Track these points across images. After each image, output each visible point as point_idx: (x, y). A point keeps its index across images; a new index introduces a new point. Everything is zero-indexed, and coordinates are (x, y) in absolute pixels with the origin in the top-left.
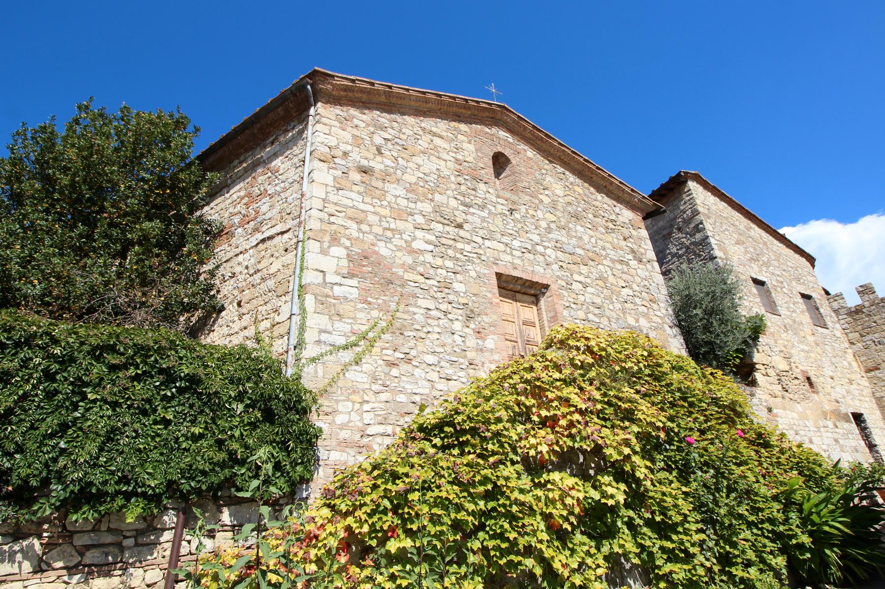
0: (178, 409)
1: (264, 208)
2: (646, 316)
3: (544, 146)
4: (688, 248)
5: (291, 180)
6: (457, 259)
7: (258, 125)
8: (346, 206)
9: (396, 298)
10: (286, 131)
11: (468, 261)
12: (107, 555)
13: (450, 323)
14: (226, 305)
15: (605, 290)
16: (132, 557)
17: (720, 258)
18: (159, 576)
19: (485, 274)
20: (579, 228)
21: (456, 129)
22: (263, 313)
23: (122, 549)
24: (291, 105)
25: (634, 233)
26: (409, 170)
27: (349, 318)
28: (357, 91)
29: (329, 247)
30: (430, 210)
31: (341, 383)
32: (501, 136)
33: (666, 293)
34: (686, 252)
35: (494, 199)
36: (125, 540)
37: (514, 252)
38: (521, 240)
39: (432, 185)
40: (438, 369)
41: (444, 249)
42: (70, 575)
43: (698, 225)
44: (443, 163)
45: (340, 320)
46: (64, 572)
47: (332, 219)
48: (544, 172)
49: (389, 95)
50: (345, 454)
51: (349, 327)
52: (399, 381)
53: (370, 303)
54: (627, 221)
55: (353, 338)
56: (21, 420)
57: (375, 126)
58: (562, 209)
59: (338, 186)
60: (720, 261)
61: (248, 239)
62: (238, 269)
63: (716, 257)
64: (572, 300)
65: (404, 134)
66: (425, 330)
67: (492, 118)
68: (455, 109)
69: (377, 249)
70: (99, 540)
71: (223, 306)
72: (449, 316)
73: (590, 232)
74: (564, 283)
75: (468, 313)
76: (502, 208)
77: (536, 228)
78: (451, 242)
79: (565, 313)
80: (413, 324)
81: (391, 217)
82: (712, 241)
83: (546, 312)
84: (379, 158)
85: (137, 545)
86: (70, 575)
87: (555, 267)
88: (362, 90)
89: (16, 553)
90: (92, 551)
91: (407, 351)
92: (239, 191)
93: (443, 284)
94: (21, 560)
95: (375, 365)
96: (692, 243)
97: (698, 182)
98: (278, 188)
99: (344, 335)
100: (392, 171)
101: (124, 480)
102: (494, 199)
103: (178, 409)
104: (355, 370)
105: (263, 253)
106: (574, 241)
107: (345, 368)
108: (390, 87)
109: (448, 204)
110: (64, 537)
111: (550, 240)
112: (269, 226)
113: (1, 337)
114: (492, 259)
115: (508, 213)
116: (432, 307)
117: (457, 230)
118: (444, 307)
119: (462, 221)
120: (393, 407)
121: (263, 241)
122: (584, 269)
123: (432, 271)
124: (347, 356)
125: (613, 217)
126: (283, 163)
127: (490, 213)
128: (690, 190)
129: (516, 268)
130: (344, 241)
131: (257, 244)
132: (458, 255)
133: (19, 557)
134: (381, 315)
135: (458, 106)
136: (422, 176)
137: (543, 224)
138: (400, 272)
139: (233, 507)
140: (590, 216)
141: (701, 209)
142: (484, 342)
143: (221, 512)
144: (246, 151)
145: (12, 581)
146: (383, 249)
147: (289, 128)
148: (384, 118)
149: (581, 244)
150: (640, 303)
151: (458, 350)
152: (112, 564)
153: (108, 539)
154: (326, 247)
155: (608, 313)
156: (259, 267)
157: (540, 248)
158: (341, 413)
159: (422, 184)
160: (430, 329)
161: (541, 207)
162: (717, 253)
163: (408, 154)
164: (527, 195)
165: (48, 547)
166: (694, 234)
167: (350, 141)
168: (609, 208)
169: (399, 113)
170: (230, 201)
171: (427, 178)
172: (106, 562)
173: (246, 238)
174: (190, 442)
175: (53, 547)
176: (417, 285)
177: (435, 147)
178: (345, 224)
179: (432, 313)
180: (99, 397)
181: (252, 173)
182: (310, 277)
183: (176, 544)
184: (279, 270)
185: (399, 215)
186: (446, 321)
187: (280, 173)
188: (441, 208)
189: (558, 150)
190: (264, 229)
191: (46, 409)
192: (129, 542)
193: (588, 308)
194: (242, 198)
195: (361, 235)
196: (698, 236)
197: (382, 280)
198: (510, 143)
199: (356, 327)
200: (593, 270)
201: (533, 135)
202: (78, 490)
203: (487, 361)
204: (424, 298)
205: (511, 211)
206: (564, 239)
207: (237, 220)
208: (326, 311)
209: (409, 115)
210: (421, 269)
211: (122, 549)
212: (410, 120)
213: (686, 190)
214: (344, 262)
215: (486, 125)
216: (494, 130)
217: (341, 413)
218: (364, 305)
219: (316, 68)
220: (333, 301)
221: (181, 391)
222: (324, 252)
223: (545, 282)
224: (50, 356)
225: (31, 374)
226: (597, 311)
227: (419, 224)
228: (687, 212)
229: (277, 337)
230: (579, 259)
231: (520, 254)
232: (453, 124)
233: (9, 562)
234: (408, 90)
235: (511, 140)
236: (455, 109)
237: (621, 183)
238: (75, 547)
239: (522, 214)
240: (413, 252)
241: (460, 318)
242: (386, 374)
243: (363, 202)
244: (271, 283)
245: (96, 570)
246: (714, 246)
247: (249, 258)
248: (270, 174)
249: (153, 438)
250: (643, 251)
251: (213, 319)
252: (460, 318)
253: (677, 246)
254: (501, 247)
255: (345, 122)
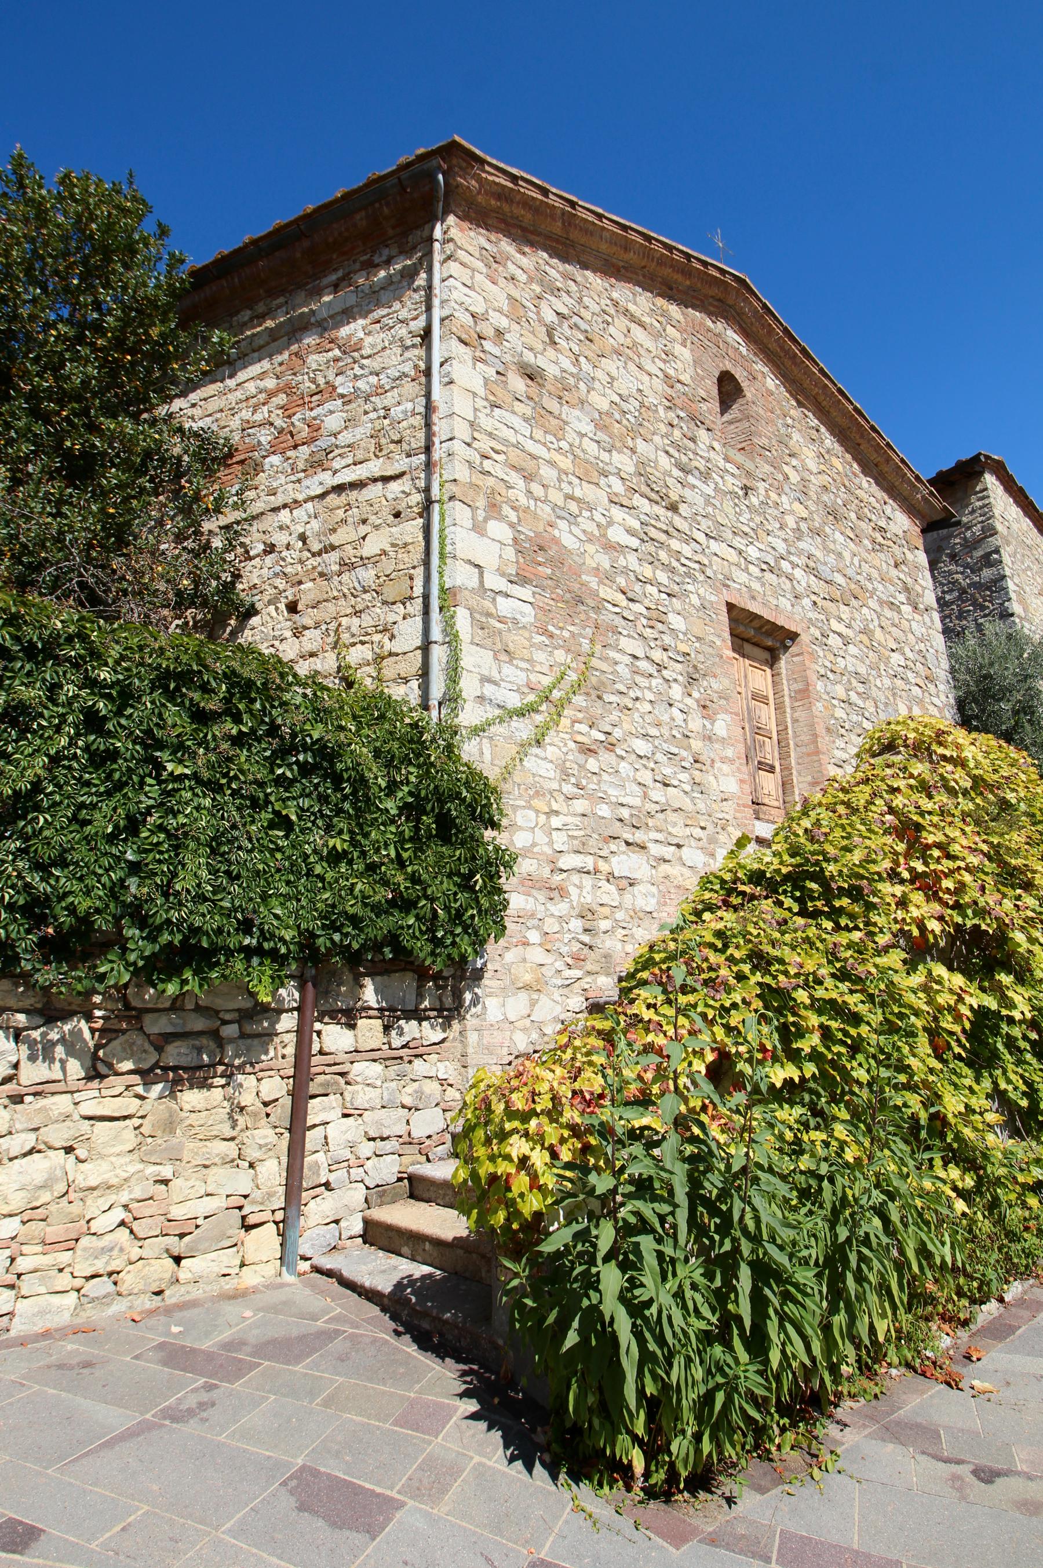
0: (306, 803)
1: (333, 423)
2: (920, 702)
3: (796, 370)
4: (963, 591)
5: (394, 373)
6: (673, 571)
7: (306, 243)
8: (505, 442)
9: (589, 631)
10: (371, 266)
11: (688, 575)
12: (199, 1050)
13: (666, 686)
14: (259, 606)
15: (871, 654)
16: (238, 1056)
17: (1019, 617)
18: (280, 1090)
19: (711, 603)
20: (837, 535)
21: (664, 314)
22: (354, 630)
23: (221, 1043)
24: (386, 211)
25: (909, 556)
26: (597, 385)
27: (522, 659)
28: (518, 203)
29: (486, 520)
30: (632, 469)
31: (517, 777)
32: (729, 340)
33: (947, 667)
34: (959, 598)
35: (721, 463)
36: (224, 1027)
37: (751, 567)
38: (762, 547)
39: (632, 420)
40: (652, 765)
41: (653, 549)
42: (147, 1084)
43: (990, 553)
44: (646, 378)
45: (510, 662)
46: (136, 1079)
47: (487, 465)
48: (790, 421)
49: (570, 220)
50: (531, 900)
51: (523, 675)
52: (599, 782)
53: (551, 636)
54: (901, 534)
55: (531, 698)
56: (55, 804)
57: (541, 283)
58: (815, 498)
59: (492, 398)
60: (1017, 620)
61: (299, 481)
62: (280, 539)
63: (1012, 615)
64: (829, 665)
65: (586, 307)
66: (632, 694)
67: (720, 300)
68: (667, 271)
69: (556, 533)
70: (184, 1024)
71: (253, 605)
72: (665, 672)
73: (851, 545)
74: (818, 634)
75: (691, 670)
76: (732, 483)
77: (781, 528)
78: (663, 537)
79: (820, 686)
80: (614, 682)
81: (574, 474)
82: (1011, 585)
83: (788, 680)
84: (551, 352)
85: (243, 1035)
86: (147, 1084)
87: (806, 602)
88: (527, 203)
89: (54, 1044)
90: (176, 1044)
91: (608, 729)
92: (262, 376)
93: (654, 614)
94: (64, 1056)
95: (564, 750)
96: (973, 585)
97: (998, 478)
98: (361, 384)
99: (517, 691)
100: (572, 381)
101: (246, 926)
102: (721, 463)
103: (306, 803)
104: (536, 756)
105: (340, 513)
106: (831, 559)
107: (524, 747)
108: (573, 204)
109: (656, 462)
110: (128, 1019)
111: (800, 553)
112: (350, 461)
113: (3, 637)
114: (721, 577)
115: (741, 493)
116: (640, 654)
117: (669, 514)
118: (658, 655)
119: (677, 498)
120: (593, 824)
121: (339, 489)
122: (845, 612)
123: (637, 587)
124: (523, 729)
125: (882, 523)
126: (369, 334)
127: (716, 489)
128: (986, 489)
129: (753, 598)
130: (506, 510)
131: (322, 496)
132: (675, 564)
133: (60, 1051)
134: (569, 660)
135: (673, 265)
136: (617, 399)
137: (790, 521)
138: (593, 583)
139: (378, 978)
140: (853, 516)
141: (999, 527)
142: (712, 724)
143: (362, 986)
144: (272, 294)
145: (53, 1094)
146: (567, 536)
147: (377, 260)
148: (555, 269)
149: (841, 565)
150: (913, 681)
151: (678, 736)
152: (208, 1066)
153: (199, 1024)
154: (480, 519)
155: (874, 692)
156: (335, 539)
157: (785, 565)
158: (521, 828)
159: (617, 416)
160: (639, 694)
161: (786, 489)
162: (1015, 607)
163: (593, 351)
164: (767, 462)
165: (107, 1033)
166: (980, 569)
167: (505, 308)
168: (877, 505)
169: (579, 263)
170: (239, 395)
171: (625, 406)
172: (200, 1063)
173: (293, 478)
174: (325, 864)
175: (114, 1035)
176: (617, 610)
177: (635, 344)
178: (506, 478)
179: (640, 664)
180: (187, 771)
181: (289, 344)
182: (460, 576)
183: (303, 1035)
184: (384, 553)
185: (587, 472)
186: (661, 681)
187: (364, 352)
188: (648, 469)
189: (818, 383)
190: (337, 464)
191: (96, 786)
192: (230, 1031)
193: (849, 681)
194: (271, 394)
195: (532, 502)
196: (987, 574)
197: (568, 595)
198: (743, 357)
199: (534, 678)
200: (857, 615)
201: (782, 348)
202: (180, 942)
203: (717, 759)
204: (629, 636)
205: (746, 489)
206: (818, 554)
207: (265, 437)
208: (488, 642)
209: (594, 271)
210: (621, 581)
211: (221, 1043)
212: (595, 281)
213: (978, 489)
214: (510, 553)
215: (710, 314)
216: (720, 326)
217: (521, 828)
218: (543, 638)
219: (457, 138)
220: (498, 625)
221: (305, 770)
222: (478, 529)
223: (793, 629)
224: (91, 683)
225: (64, 715)
226: (861, 688)
227: (616, 494)
228: (974, 529)
229: (394, 680)
230: (838, 593)
231: (759, 574)
232: (660, 302)
233: (44, 1061)
234: (600, 216)
235: (743, 350)
236: (667, 271)
237: (902, 461)
238: (148, 1036)
239: (761, 498)
240: (611, 547)
241: (680, 678)
242: (580, 766)
243: (531, 438)
244: (367, 575)
245: (186, 1076)
246: (1013, 595)
247: (306, 519)
248: (337, 352)
249: (272, 852)
250: (919, 590)
251: (229, 629)
252: (680, 678)
253: (943, 585)
254: (732, 556)
255: (495, 265)
